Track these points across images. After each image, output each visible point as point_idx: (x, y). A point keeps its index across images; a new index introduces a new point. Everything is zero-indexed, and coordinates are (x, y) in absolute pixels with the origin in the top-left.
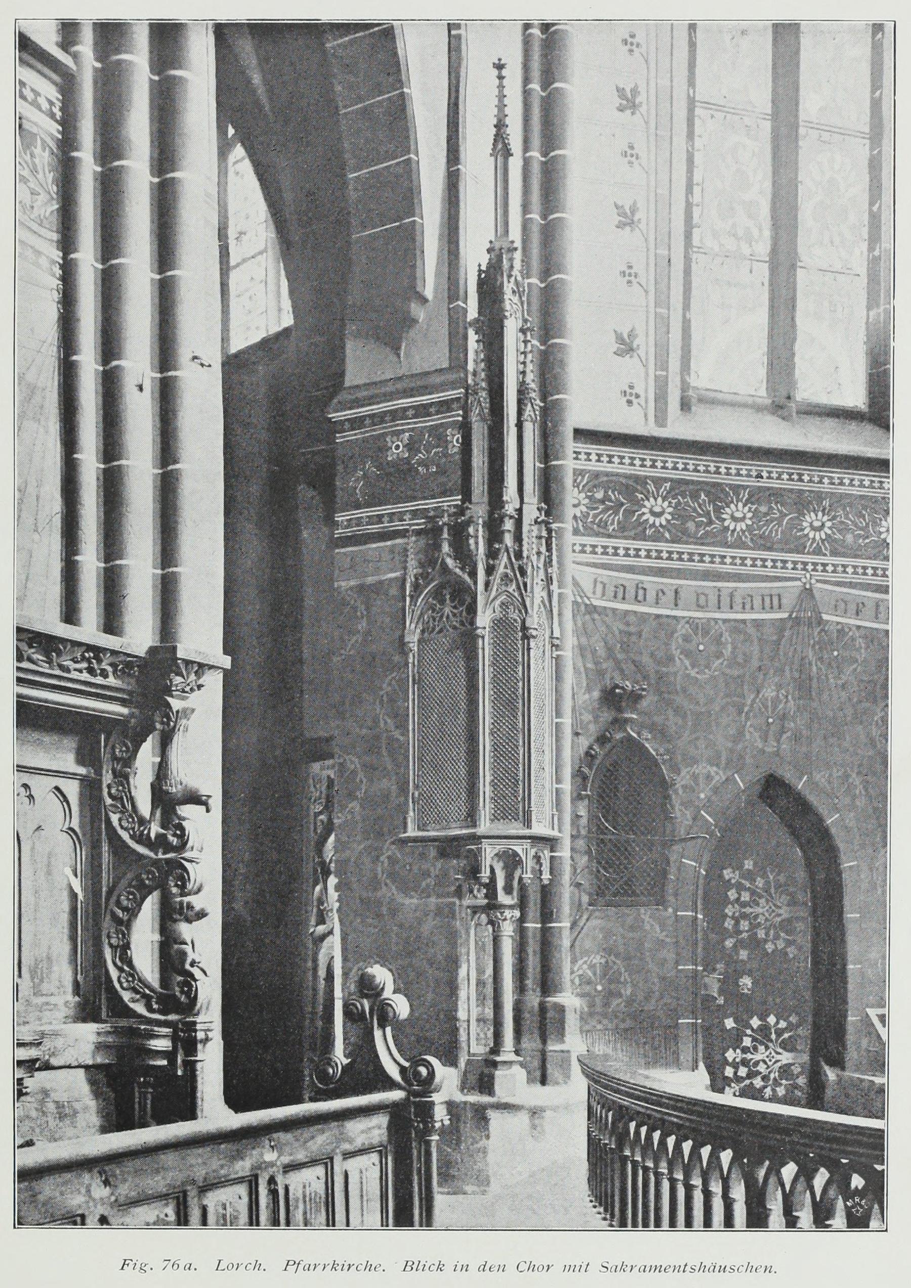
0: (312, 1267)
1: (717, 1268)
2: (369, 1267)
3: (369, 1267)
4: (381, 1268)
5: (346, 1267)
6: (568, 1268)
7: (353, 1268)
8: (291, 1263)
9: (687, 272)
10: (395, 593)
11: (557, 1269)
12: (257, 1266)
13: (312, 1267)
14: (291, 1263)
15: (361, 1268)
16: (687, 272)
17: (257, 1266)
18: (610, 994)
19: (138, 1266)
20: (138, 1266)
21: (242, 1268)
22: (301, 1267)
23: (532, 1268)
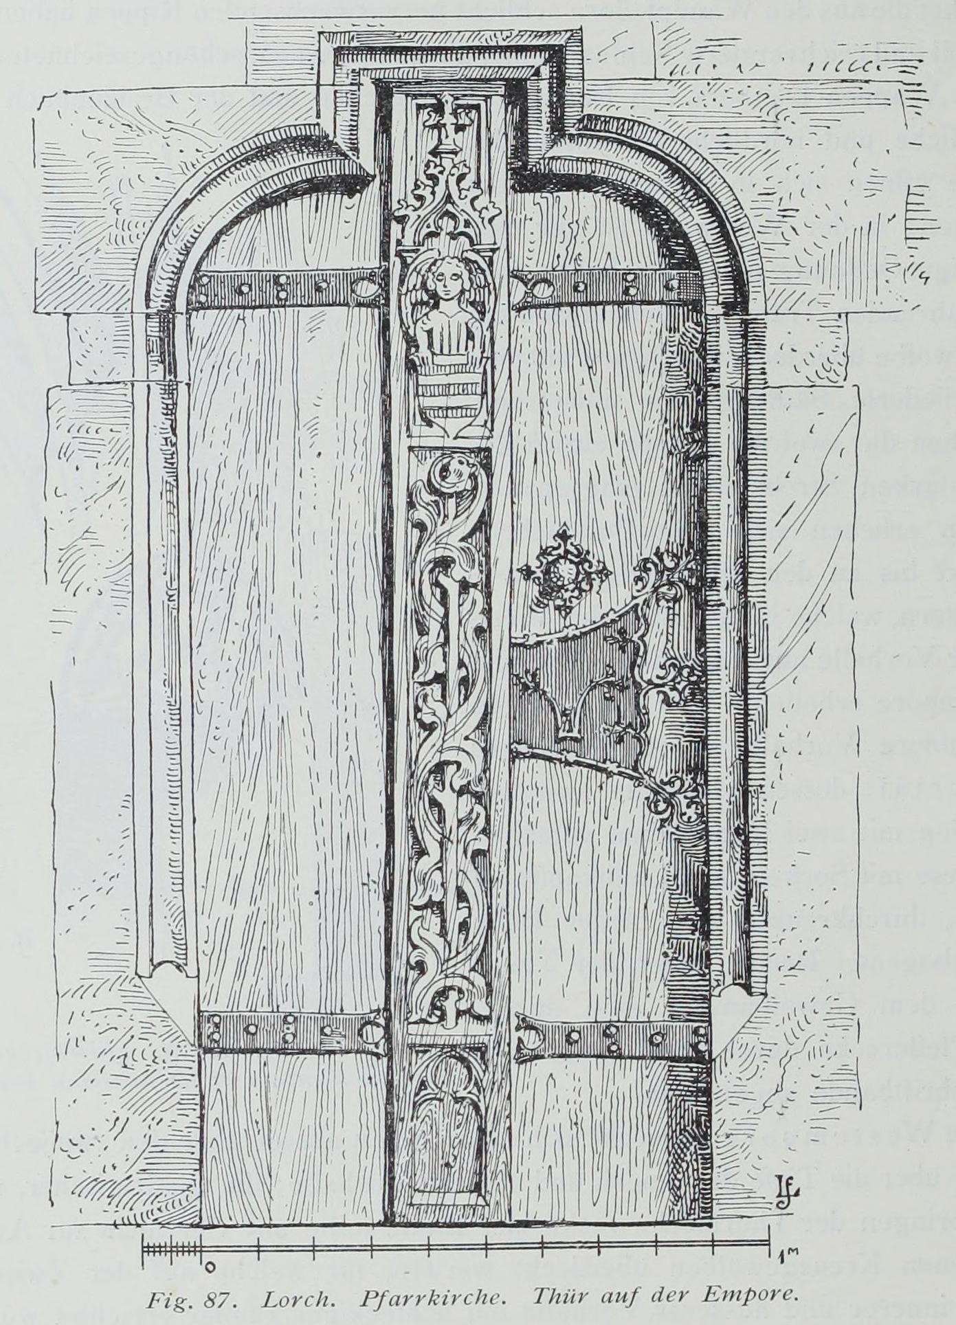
0: (402, 1300)
1: (614, 1297)
2: (482, 1297)
3: (482, 1297)
4: (500, 1300)
5: (450, 1300)
6: (608, 1299)
7: (460, 1300)
8: (372, 1295)
9: (386, 415)
10: (631, 1076)
11: (593, 1300)
12: (322, 1300)
13: (402, 1300)
14: (372, 1295)
15: (472, 1299)
16: (386, 415)
17: (322, 1300)
18: (678, 950)
19: (172, 1303)
20: (172, 1303)
21: (301, 1303)
22: (386, 1300)
23: (555, 1298)
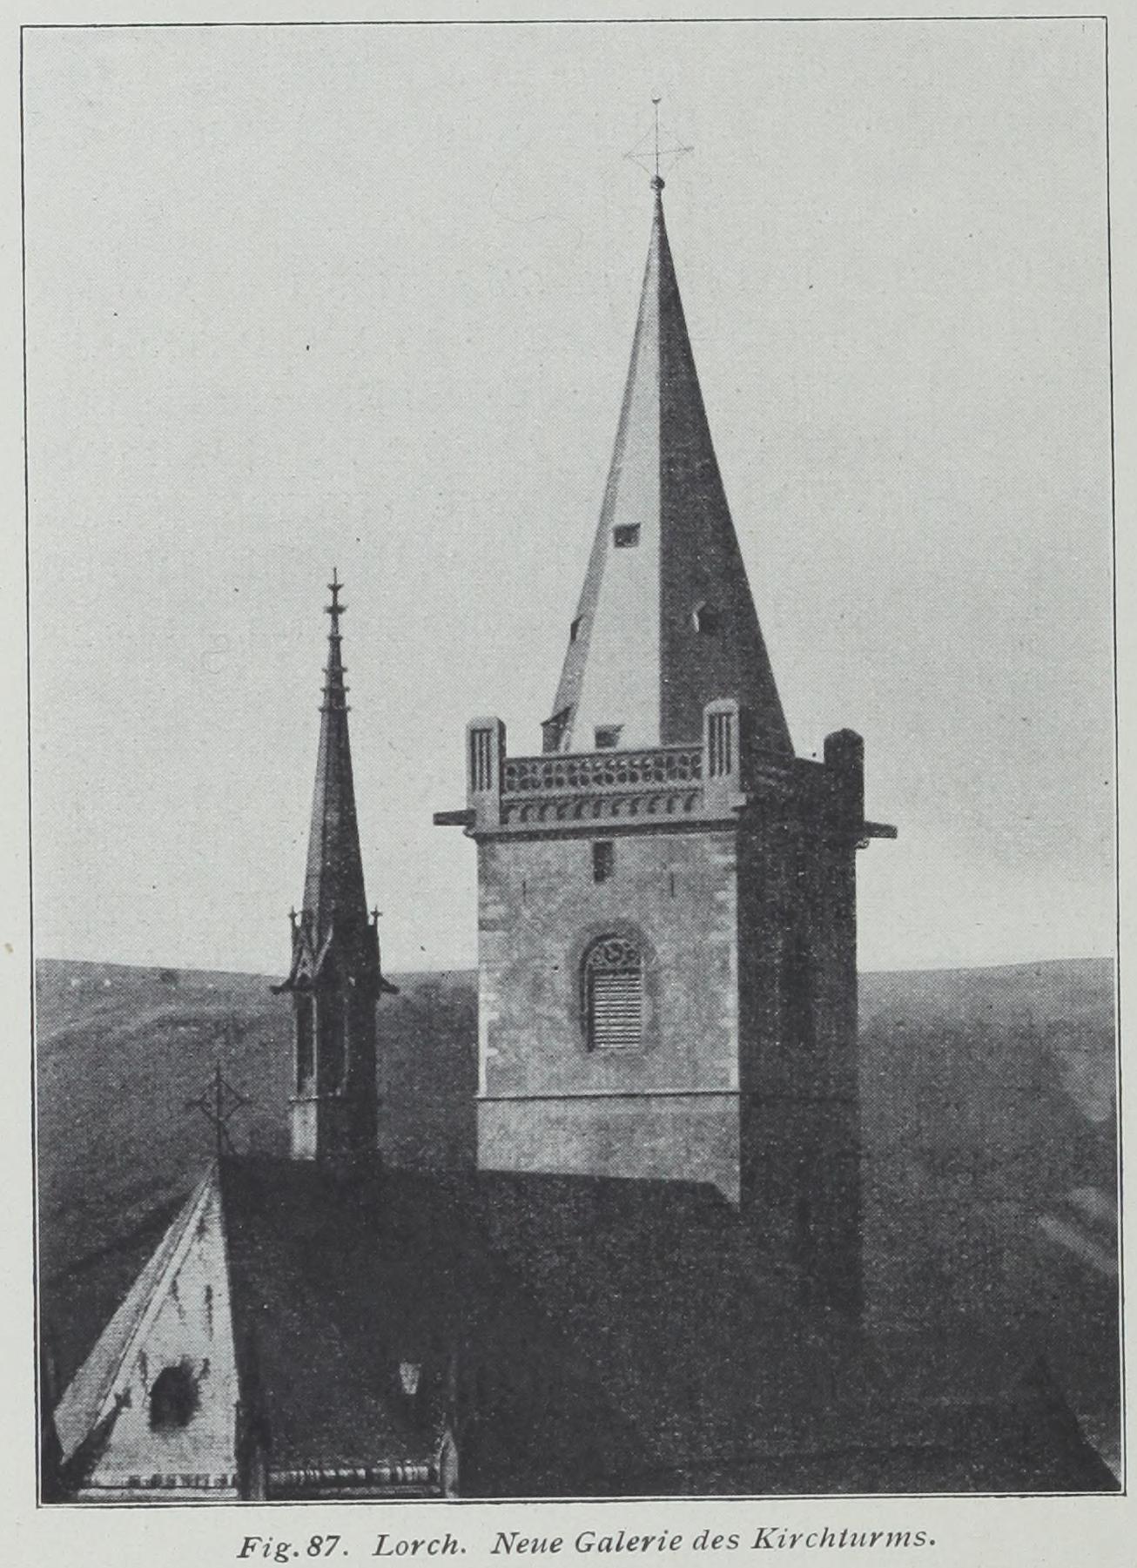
5: (788, 1541)
7: (801, 1542)
12: (450, 1545)
15: (816, 1540)
17: (450, 1545)
20: (273, 1550)
21: (422, 1549)
